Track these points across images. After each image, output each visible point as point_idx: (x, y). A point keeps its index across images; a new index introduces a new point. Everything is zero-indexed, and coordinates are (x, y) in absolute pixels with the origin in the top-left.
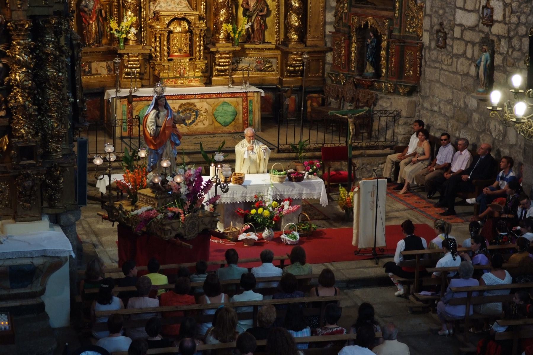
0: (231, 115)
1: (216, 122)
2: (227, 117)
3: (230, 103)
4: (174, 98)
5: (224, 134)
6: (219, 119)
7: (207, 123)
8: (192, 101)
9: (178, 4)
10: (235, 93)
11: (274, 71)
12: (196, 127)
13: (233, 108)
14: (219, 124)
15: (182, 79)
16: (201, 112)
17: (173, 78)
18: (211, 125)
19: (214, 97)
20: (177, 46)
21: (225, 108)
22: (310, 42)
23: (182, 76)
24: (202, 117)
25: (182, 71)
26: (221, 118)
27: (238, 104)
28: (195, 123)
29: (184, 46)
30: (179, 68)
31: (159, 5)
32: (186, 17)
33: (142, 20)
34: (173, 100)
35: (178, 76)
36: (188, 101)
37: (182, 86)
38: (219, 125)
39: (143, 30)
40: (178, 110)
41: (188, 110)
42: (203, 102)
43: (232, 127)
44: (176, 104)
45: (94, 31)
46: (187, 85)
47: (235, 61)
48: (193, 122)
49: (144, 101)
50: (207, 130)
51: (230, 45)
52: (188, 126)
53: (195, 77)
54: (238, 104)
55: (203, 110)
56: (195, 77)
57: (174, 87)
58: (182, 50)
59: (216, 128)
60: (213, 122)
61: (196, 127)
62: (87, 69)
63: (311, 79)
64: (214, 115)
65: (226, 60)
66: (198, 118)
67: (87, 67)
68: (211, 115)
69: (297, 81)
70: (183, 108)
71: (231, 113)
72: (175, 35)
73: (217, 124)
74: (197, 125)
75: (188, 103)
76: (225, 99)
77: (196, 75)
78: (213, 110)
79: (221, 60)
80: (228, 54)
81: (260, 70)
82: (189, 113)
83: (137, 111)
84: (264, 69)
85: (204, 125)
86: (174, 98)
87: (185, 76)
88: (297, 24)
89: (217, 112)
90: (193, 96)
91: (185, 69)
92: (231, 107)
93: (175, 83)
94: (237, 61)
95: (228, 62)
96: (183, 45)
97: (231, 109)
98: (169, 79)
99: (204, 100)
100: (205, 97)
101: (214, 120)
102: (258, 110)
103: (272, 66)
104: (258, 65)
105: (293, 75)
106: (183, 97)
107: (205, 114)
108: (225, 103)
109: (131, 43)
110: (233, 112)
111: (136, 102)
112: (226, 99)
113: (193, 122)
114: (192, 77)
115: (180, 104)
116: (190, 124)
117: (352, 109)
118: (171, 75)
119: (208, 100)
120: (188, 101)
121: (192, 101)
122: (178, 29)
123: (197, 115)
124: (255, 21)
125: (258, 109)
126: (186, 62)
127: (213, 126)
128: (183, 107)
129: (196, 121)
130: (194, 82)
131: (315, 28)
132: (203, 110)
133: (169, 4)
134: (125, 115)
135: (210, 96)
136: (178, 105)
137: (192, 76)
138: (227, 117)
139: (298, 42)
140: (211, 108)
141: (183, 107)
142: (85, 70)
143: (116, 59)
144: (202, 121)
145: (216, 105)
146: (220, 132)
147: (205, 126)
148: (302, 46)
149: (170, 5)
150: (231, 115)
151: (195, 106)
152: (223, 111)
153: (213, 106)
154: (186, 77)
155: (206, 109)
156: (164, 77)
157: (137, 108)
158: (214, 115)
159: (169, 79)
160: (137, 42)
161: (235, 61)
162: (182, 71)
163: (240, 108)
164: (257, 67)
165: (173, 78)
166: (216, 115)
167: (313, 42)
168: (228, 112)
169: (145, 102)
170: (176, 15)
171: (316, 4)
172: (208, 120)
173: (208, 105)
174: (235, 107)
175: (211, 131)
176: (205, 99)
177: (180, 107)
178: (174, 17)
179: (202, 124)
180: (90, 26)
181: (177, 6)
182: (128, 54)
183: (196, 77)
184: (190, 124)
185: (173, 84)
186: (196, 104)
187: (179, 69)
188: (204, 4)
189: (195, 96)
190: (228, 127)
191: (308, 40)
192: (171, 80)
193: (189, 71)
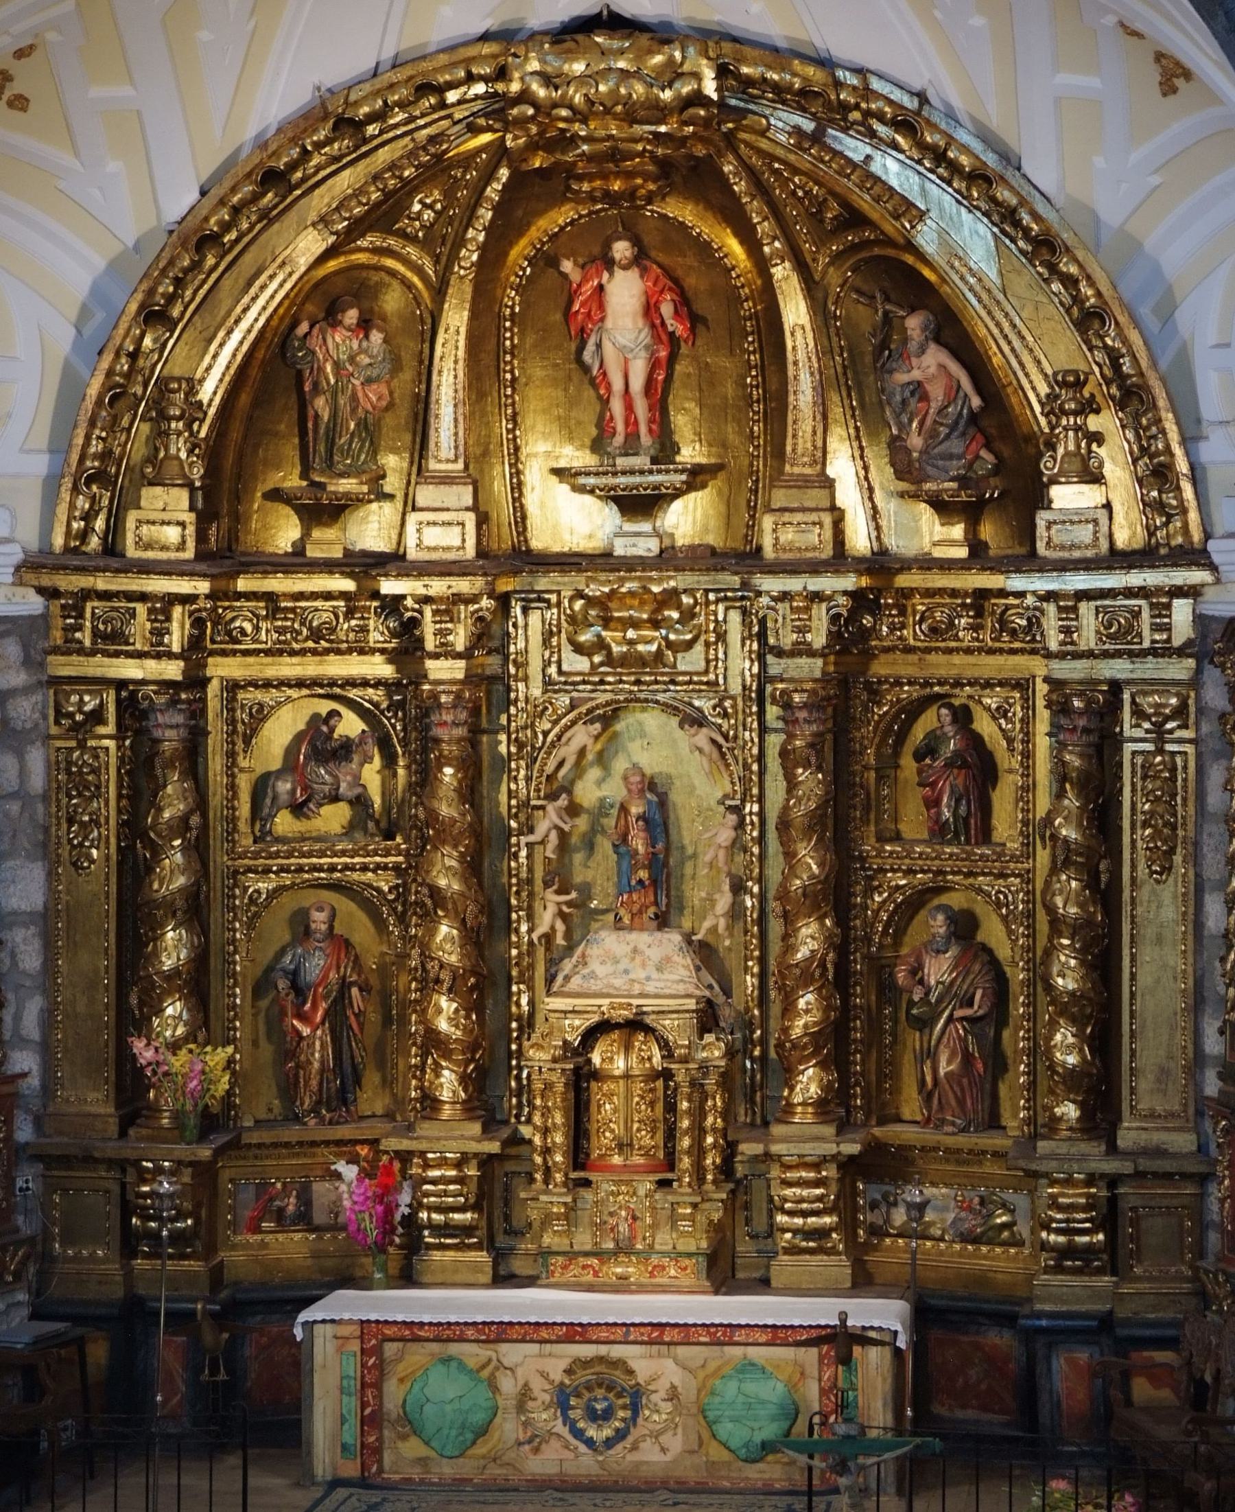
0: (774, 1419)
1: (714, 1443)
2: (756, 1425)
3: (769, 1369)
4: (544, 1334)
5: (741, 1492)
6: (725, 1429)
7: (675, 1443)
8: (617, 1351)
9: (659, 969)
10: (784, 1327)
11: (1020, 1244)
12: (631, 1457)
13: (780, 1387)
14: (726, 1452)
15: (622, 1258)
16: (654, 1397)
17: (587, 1254)
18: (692, 1452)
19: (702, 1339)
20: (612, 1131)
21: (750, 1387)
22: (1133, 1134)
23: (623, 1250)
24: (656, 1417)
25: (623, 1228)
26: (730, 1425)
27: (802, 1374)
28: (630, 1439)
29: (639, 1130)
30: (611, 1214)
31: (585, 971)
32: (648, 1020)
33: (514, 1025)
34: (541, 1342)
35: (611, 1245)
36: (603, 1350)
37: (622, 1286)
38: (725, 1455)
39: (514, 1062)
40: (562, 1383)
41: (600, 1385)
42: (660, 1355)
43: (778, 1467)
44: (553, 1361)
45: (316, 1065)
46: (641, 1285)
47: (878, 1197)
48: (621, 1435)
49: (427, 1340)
50: (677, 1474)
51: (829, 1130)
52: (601, 1453)
53: (676, 1255)
54: (802, 1374)
55: (662, 1386)
56: (676, 1255)
57: (590, 1288)
58: (631, 1145)
59: (712, 1465)
60: (701, 1445)
61: (631, 1457)
62: (291, 1205)
63: (1143, 1287)
64: (703, 1411)
65: (805, 1193)
66: (640, 1421)
67: (293, 1200)
68: (694, 1410)
69: (1096, 1294)
70: (584, 1376)
71: (772, 1409)
72: (605, 1087)
73: (716, 1453)
74: (634, 1448)
75: (601, 1359)
76: (750, 1349)
77: (680, 1248)
78: (699, 1391)
79: (789, 1192)
80: (816, 1166)
81: (966, 1238)
82: (606, 1399)
83: (401, 1380)
84: (983, 1233)
85: (664, 1450)
86: (544, 1334)
87: (639, 1246)
88: (1072, 1060)
89: (717, 1400)
90: (620, 1332)
91: (635, 1218)
92: (771, 1383)
93: (596, 1274)
94: (885, 1196)
95: (820, 1199)
96: (636, 1126)
97: (772, 1391)
98: (572, 1255)
99: (664, 1348)
100: (667, 1339)
101: (706, 1435)
102: (885, 1405)
103: (1013, 1223)
104: (963, 1214)
105: (1070, 1268)
106: (581, 1334)
107: (667, 1407)
108: (748, 1368)
109: (447, 1112)
110: (781, 1406)
111: (400, 1345)
112: (752, 1351)
113: (621, 1435)
114: (663, 1254)
115: (569, 1361)
116: (609, 1443)
117: (853, 1433)
118: (584, 1240)
119: (681, 1351)
120: (603, 1350)
121: (617, 1351)
122: (619, 1065)
123: (635, 1408)
124: (945, 1040)
125: (885, 1399)
126: (642, 1192)
127: (700, 1460)
128: (580, 1373)
129: (635, 1434)
130: (673, 1273)
131: (1159, 1081)
132: (662, 1386)
133: (621, 967)
134: (349, 1395)
135: (687, 1335)
136: (564, 1364)
137: (665, 1248)
138: (756, 1425)
139: (1082, 1130)
140: (694, 1384)
141: (580, 1373)
142: (281, 1210)
143: (161, 1183)
144: (656, 1435)
145: (714, 1374)
146: (726, 1484)
147: (668, 1457)
148: (1095, 1149)
149: (626, 972)
150: (774, 1419)
151: (631, 1372)
152: (741, 1399)
153: (701, 1375)
154: (638, 1253)
155: (673, 1387)
156: (555, 1249)
157: (401, 1369)
158: (703, 1411)
159: (572, 1255)
160: (465, 1110)
161: (878, 1197)
162: (623, 1228)
163: (812, 1391)
164: (959, 1224)
165: (587, 1254)
166: (711, 1415)
167: (1144, 1136)
168: (763, 1402)
169: (435, 1347)
170: (604, 1009)
171: (1158, 981)
172: (680, 1430)
173: (680, 1370)
174: (792, 1387)
175: (692, 1476)
176: (669, 1344)
177: (569, 1372)
178: (596, 1018)
179: (657, 1448)
180: (304, 1044)
181: (655, 975)
182: (422, 1154)
183: (680, 1254)
184: (609, 1443)
185: (589, 1278)
186: (634, 1365)
187: (612, 1221)
188: (756, 970)
189: (626, 1331)
190: (760, 1466)
191: (1126, 1124)
192: (582, 1261)
193: (654, 1227)
